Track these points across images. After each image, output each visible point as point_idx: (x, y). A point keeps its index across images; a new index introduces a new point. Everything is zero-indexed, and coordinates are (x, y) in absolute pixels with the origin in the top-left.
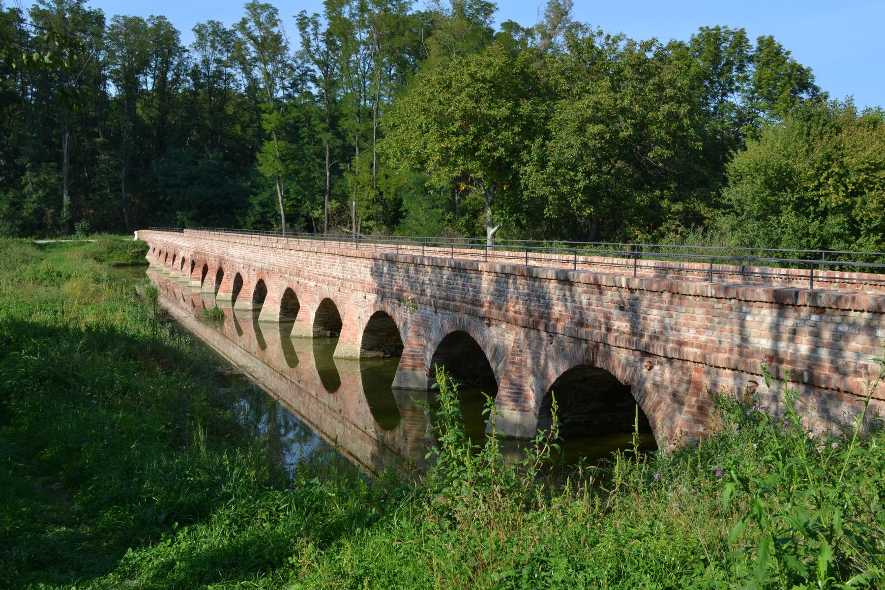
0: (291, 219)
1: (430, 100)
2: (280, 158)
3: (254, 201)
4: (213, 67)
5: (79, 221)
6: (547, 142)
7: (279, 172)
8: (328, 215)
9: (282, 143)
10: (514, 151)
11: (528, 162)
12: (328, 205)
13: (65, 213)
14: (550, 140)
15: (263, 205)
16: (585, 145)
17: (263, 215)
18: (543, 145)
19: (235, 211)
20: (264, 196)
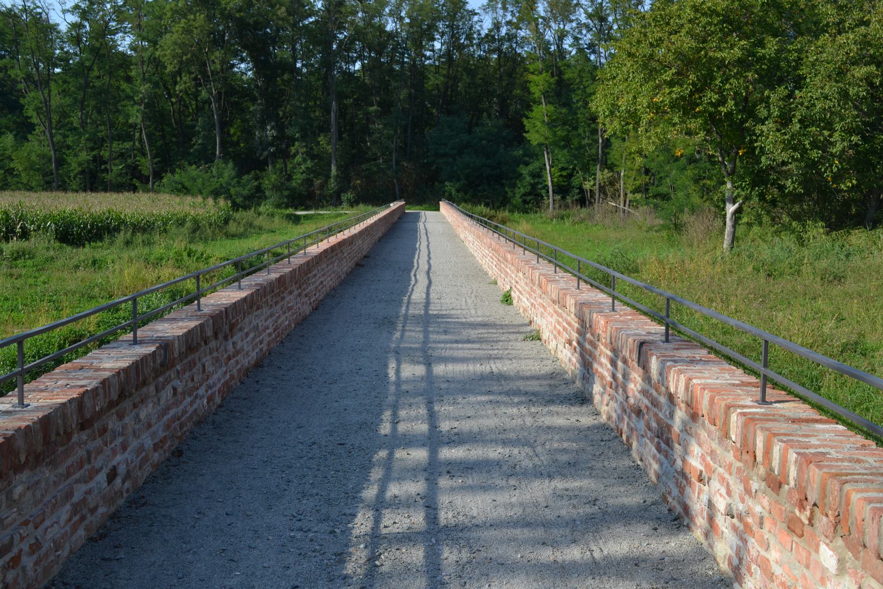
0: (562, 190)
1: (639, 42)
2: (548, 124)
3: (524, 170)
4: (504, 31)
5: (345, 192)
6: (797, 92)
7: (546, 138)
8: (600, 187)
9: (551, 108)
10: (747, 107)
11: (766, 119)
12: (599, 176)
13: (332, 184)
14: (800, 88)
15: (534, 175)
16: (844, 95)
17: (533, 186)
18: (791, 95)
19: (504, 181)
20: (534, 166)
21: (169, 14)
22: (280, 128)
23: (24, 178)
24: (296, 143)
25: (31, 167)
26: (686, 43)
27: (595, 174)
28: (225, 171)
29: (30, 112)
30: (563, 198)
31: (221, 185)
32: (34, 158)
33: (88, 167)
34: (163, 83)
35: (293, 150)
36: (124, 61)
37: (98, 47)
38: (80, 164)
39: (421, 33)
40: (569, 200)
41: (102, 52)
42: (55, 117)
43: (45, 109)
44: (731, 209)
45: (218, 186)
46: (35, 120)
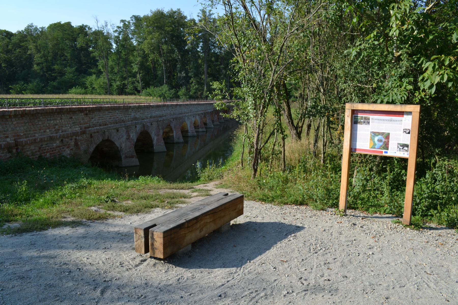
21: (147, 33)
22: (187, 73)
23: (98, 91)
24: (192, 79)
25: (100, 87)
28: (165, 88)
29: (100, 67)
32: (101, 83)
34: (145, 57)
36: (134, 49)
38: (117, 86)
42: (110, 69)
45: (161, 93)
46: (102, 70)
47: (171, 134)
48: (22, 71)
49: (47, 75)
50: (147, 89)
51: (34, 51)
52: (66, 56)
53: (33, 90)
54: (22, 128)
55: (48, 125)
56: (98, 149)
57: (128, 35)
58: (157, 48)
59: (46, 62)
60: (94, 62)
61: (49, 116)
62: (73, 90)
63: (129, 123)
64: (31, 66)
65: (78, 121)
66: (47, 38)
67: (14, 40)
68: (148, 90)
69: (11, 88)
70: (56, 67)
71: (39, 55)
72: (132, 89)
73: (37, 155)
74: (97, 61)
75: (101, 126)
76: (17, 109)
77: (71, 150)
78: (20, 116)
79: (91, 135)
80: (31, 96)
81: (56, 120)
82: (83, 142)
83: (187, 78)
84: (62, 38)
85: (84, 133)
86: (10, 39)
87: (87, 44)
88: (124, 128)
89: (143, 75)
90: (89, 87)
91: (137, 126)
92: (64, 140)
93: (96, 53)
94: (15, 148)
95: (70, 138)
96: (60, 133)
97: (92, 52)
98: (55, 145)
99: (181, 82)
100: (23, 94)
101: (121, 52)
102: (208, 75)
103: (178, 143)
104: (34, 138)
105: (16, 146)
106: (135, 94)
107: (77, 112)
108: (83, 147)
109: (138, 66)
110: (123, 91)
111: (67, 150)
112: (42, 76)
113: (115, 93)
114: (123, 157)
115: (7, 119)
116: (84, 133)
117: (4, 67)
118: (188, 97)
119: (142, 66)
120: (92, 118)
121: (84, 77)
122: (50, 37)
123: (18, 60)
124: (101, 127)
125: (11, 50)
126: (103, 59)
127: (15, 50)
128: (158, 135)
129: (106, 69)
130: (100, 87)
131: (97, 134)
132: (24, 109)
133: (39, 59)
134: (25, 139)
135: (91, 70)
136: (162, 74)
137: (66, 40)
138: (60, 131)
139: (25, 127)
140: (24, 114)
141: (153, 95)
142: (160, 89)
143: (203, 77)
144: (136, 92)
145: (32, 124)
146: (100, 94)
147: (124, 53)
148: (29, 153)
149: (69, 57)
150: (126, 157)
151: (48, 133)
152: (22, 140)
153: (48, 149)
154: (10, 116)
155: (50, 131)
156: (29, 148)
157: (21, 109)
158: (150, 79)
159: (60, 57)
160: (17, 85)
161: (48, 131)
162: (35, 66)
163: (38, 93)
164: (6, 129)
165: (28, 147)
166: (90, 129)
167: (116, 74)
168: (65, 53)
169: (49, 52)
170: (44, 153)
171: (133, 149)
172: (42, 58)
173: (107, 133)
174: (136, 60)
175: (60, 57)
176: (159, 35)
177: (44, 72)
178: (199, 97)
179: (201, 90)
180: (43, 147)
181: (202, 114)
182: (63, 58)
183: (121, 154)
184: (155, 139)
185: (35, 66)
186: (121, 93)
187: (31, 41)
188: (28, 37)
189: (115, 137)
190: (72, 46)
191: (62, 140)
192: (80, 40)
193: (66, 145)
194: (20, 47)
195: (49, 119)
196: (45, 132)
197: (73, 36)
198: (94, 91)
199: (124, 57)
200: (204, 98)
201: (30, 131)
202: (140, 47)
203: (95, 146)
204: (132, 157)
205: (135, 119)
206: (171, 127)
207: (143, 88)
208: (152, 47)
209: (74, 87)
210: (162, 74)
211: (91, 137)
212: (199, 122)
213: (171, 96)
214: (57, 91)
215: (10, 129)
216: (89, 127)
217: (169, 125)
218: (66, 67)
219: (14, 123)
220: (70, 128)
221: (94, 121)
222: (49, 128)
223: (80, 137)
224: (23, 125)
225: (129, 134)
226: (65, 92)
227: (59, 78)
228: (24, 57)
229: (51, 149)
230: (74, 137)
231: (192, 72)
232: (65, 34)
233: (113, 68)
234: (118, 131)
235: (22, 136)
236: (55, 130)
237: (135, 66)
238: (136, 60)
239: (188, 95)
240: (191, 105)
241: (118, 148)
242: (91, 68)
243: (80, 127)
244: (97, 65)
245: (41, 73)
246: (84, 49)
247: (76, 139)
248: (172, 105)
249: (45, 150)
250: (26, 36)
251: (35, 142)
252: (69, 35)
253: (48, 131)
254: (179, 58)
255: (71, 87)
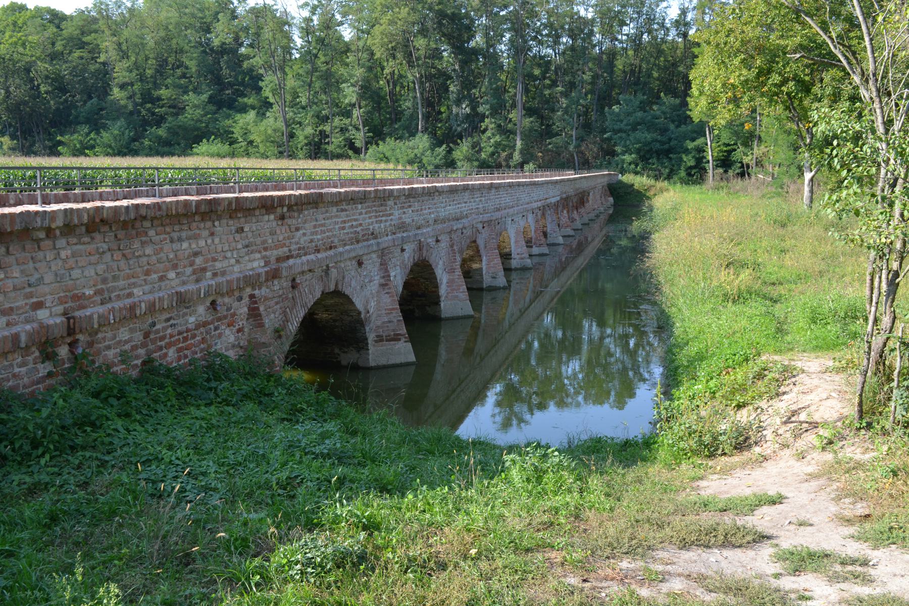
13: (517, 157)
20: (699, 142)
21: (379, 8)
22: (474, 105)
24: (486, 120)
26: (752, 32)
27: (752, 149)
28: (422, 142)
29: (267, 93)
30: (726, 172)
31: (416, 155)
32: (269, 132)
33: (313, 139)
34: (373, 67)
35: (483, 125)
36: (347, 49)
37: (323, 38)
38: (306, 138)
39: (611, 20)
40: (731, 173)
41: (326, 41)
42: (289, 98)
43: (278, 90)
44: (808, 176)
45: (412, 156)
46: (272, 100)
47: (475, 266)
48: (85, 102)
49: (144, 112)
50: (377, 145)
51: (113, 54)
52: (187, 68)
53: (110, 147)
54: (90, 272)
55: (171, 256)
56: (309, 322)
57: (333, 15)
58: (403, 47)
59: (141, 80)
60: (254, 82)
61: (177, 228)
62: (204, 147)
63: (386, 240)
64: (105, 91)
65: (258, 241)
66: (143, 26)
67: (69, 30)
68: (382, 147)
69: (60, 143)
70: (163, 92)
71: (125, 64)
72: (343, 143)
73: (137, 357)
74: (260, 78)
75: (318, 251)
76: (75, 206)
77: (239, 331)
78: (83, 229)
79: (294, 280)
80: (107, 162)
81: (196, 237)
82: (272, 303)
83: (474, 121)
84: (178, 24)
85: (274, 275)
86: (58, 27)
87: (237, 39)
88: (374, 256)
89: (369, 112)
90: (240, 140)
91: (405, 247)
92: (219, 301)
93: (257, 58)
94: (65, 345)
95: (237, 294)
96: (209, 281)
97: (248, 57)
98: (192, 319)
99: (459, 129)
100: (86, 155)
101: (316, 56)
102: (524, 112)
103: (492, 289)
104: (128, 302)
105: (69, 335)
106: (348, 157)
107: (257, 212)
108: (271, 320)
109: (356, 89)
110: (319, 148)
111: (227, 332)
112: (131, 113)
113: (301, 154)
114: (371, 337)
115: (38, 241)
116: (274, 275)
117: (46, 93)
118: (476, 163)
119: (367, 91)
120: (297, 229)
121: (228, 117)
122: (150, 22)
123: (76, 76)
124: (319, 256)
125: (62, 53)
126: (274, 72)
127: (71, 52)
128: (452, 271)
129: (281, 98)
130: (268, 140)
131: (308, 276)
132: (98, 204)
133: (125, 73)
134: (101, 309)
135: (246, 100)
136: (415, 108)
137: (186, 28)
138: (209, 274)
139: (101, 268)
140: (97, 223)
141: (393, 159)
142: (411, 144)
143: (510, 116)
144: (350, 152)
145: (124, 255)
146: (265, 156)
147: (323, 59)
148: (111, 354)
149: (194, 70)
150: (379, 339)
151: (173, 283)
152: (88, 312)
153: (171, 336)
154: (49, 231)
155: (178, 274)
156: (114, 337)
157: (89, 205)
158: (385, 120)
159: (173, 69)
160: (75, 136)
161: (172, 275)
162: (116, 90)
163: (121, 153)
164: (37, 276)
165: (109, 335)
166: (291, 262)
167: (303, 108)
168: (184, 60)
169: (147, 59)
170: (161, 348)
171: (397, 316)
172: (131, 71)
173: (334, 273)
174: (351, 76)
175: (173, 69)
176: (409, 14)
177: (136, 104)
178: (504, 163)
179: (505, 146)
180: (157, 332)
181: (539, 209)
182: (179, 72)
183: (367, 329)
184: (445, 281)
185: (116, 90)
186: (316, 154)
187: (107, 32)
188: (101, 22)
189: (353, 283)
190: (201, 44)
191: (213, 303)
192: (221, 28)
193: (225, 317)
194: (82, 45)
195: (175, 235)
196: (161, 279)
197: (203, 18)
198: (251, 150)
199: (324, 68)
200: (515, 167)
201: (115, 278)
202: (361, 44)
203: (302, 314)
204: (396, 338)
205: (402, 227)
206: (477, 247)
207: (368, 143)
208: (391, 42)
209: (205, 140)
210: (415, 108)
211: (294, 286)
212: (533, 229)
213: (437, 161)
214: (166, 149)
215: (48, 278)
216: (288, 258)
217: (475, 242)
218: (186, 92)
219: (63, 254)
220: (238, 262)
221: (302, 238)
222: (175, 267)
223: (264, 289)
224: (94, 259)
225: (387, 271)
226: (186, 151)
227: (170, 119)
228: (92, 68)
229: (180, 333)
230: (249, 291)
231: (487, 102)
232: (185, 14)
233: (296, 95)
234: (360, 264)
235: (90, 297)
236: (194, 272)
237: (351, 89)
238: (351, 76)
239: (477, 160)
240: (519, 184)
241: (360, 313)
242: (245, 96)
243: (263, 258)
244: (261, 88)
245: (130, 107)
246: (229, 51)
247: (252, 296)
248: (482, 186)
249: (162, 338)
250: (95, 20)
251: (131, 313)
252: (193, 16)
253: (172, 275)
254: (454, 70)
255: (198, 140)
